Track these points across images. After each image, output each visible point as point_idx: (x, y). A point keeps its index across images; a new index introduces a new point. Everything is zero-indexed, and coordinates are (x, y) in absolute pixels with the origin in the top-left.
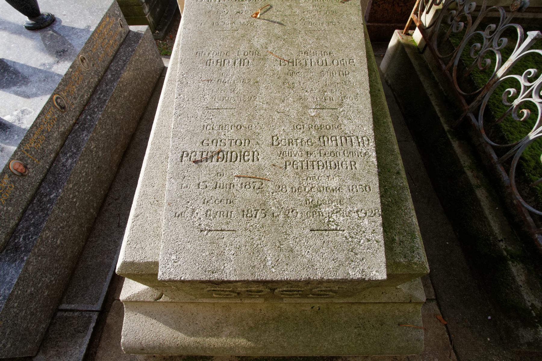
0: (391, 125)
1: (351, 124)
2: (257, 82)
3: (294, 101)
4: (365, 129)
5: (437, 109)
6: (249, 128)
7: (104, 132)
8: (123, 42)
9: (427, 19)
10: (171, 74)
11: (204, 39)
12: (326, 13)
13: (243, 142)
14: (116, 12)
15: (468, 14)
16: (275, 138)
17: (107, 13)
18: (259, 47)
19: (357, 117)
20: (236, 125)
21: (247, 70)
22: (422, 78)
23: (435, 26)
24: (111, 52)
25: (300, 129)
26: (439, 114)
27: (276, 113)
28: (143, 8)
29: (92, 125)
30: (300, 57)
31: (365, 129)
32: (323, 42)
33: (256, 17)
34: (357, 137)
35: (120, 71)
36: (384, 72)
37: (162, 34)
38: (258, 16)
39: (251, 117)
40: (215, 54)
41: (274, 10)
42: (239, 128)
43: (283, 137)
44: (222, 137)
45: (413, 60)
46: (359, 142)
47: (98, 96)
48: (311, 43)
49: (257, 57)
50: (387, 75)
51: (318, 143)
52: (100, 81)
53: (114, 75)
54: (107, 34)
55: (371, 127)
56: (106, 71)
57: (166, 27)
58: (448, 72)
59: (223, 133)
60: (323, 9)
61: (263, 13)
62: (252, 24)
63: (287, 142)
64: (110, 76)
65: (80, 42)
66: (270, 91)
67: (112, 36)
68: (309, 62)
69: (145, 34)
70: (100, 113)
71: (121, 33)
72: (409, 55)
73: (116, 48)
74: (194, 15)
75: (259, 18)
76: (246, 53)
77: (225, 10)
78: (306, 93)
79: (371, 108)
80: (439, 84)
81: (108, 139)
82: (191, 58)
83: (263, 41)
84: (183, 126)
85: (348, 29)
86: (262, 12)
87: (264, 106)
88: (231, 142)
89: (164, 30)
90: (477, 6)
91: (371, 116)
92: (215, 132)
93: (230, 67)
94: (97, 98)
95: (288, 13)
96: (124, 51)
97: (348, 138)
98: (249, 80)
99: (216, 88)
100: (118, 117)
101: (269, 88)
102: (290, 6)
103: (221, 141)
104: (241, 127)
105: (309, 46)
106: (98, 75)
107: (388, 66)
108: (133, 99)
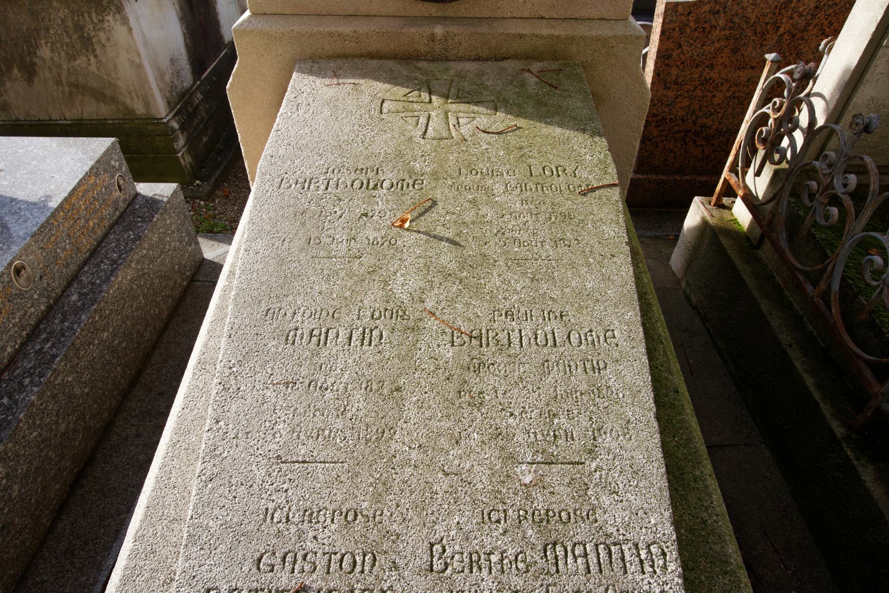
0: (713, 484)
1: (619, 505)
2: (398, 389)
3: (483, 442)
4: (653, 521)
5: (809, 381)
6: (373, 519)
7: (35, 434)
8: (117, 220)
9: (759, 184)
10: (206, 345)
11: (286, 276)
12: (550, 218)
13: (359, 559)
14: (113, 163)
15: (844, 194)
16: (437, 548)
17: (92, 168)
18: (405, 297)
19: (624, 326)
20: (344, 510)
21: (377, 357)
22: (765, 306)
23: (778, 203)
24: (87, 243)
25: (498, 521)
26: (817, 395)
27: (440, 475)
28: (175, 140)
29: (9, 422)
30: (495, 326)
31: (653, 521)
32: (545, 286)
33: (401, 227)
34: (636, 546)
35: (100, 285)
36: (679, 275)
37: (207, 187)
38: (407, 225)
39: (380, 487)
40: (308, 313)
41: (441, 211)
42: (350, 517)
43: (457, 548)
44: (310, 545)
45: (739, 263)
46: (641, 562)
47: (38, 347)
48: (519, 289)
49: (400, 324)
50: (688, 284)
51: (541, 563)
52: (50, 308)
53: (86, 294)
54: (86, 209)
55: (667, 514)
56: (69, 285)
57: (218, 173)
58: (819, 301)
59: (311, 534)
60: (543, 208)
61: (417, 218)
62: (393, 242)
63: (467, 560)
64: (74, 298)
65: (21, 233)
66: (428, 414)
67: (95, 211)
68: (515, 341)
69: (168, 202)
70: (35, 389)
71: (116, 201)
72: (729, 252)
73: (100, 233)
74: (270, 219)
75: (408, 230)
76: (377, 314)
77: (337, 209)
78: (511, 420)
79: (662, 461)
80: (805, 319)
81: (42, 450)
82: (253, 323)
83: (415, 283)
84: (216, 511)
85: (598, 258)
86: (415, 214)
87: (414, 455)
88: (330, 560)
89: (214, 178)
90: (859, 185)
91: (664, 483)
92: (293, 529)
93: (339, 348)
94: (36, 352)
95: (469, 217)
96: (118, 240)
97: (613, 548)
98: (381, 382)
99: (304, 404)
100: (77, 391)
101: (425, 405)
102: (474, 202)
103: (305, 557)
104: (356, 515)
105: (516, 297)
106: (49, 297)
107: (688, 266)
108: (120, 343)
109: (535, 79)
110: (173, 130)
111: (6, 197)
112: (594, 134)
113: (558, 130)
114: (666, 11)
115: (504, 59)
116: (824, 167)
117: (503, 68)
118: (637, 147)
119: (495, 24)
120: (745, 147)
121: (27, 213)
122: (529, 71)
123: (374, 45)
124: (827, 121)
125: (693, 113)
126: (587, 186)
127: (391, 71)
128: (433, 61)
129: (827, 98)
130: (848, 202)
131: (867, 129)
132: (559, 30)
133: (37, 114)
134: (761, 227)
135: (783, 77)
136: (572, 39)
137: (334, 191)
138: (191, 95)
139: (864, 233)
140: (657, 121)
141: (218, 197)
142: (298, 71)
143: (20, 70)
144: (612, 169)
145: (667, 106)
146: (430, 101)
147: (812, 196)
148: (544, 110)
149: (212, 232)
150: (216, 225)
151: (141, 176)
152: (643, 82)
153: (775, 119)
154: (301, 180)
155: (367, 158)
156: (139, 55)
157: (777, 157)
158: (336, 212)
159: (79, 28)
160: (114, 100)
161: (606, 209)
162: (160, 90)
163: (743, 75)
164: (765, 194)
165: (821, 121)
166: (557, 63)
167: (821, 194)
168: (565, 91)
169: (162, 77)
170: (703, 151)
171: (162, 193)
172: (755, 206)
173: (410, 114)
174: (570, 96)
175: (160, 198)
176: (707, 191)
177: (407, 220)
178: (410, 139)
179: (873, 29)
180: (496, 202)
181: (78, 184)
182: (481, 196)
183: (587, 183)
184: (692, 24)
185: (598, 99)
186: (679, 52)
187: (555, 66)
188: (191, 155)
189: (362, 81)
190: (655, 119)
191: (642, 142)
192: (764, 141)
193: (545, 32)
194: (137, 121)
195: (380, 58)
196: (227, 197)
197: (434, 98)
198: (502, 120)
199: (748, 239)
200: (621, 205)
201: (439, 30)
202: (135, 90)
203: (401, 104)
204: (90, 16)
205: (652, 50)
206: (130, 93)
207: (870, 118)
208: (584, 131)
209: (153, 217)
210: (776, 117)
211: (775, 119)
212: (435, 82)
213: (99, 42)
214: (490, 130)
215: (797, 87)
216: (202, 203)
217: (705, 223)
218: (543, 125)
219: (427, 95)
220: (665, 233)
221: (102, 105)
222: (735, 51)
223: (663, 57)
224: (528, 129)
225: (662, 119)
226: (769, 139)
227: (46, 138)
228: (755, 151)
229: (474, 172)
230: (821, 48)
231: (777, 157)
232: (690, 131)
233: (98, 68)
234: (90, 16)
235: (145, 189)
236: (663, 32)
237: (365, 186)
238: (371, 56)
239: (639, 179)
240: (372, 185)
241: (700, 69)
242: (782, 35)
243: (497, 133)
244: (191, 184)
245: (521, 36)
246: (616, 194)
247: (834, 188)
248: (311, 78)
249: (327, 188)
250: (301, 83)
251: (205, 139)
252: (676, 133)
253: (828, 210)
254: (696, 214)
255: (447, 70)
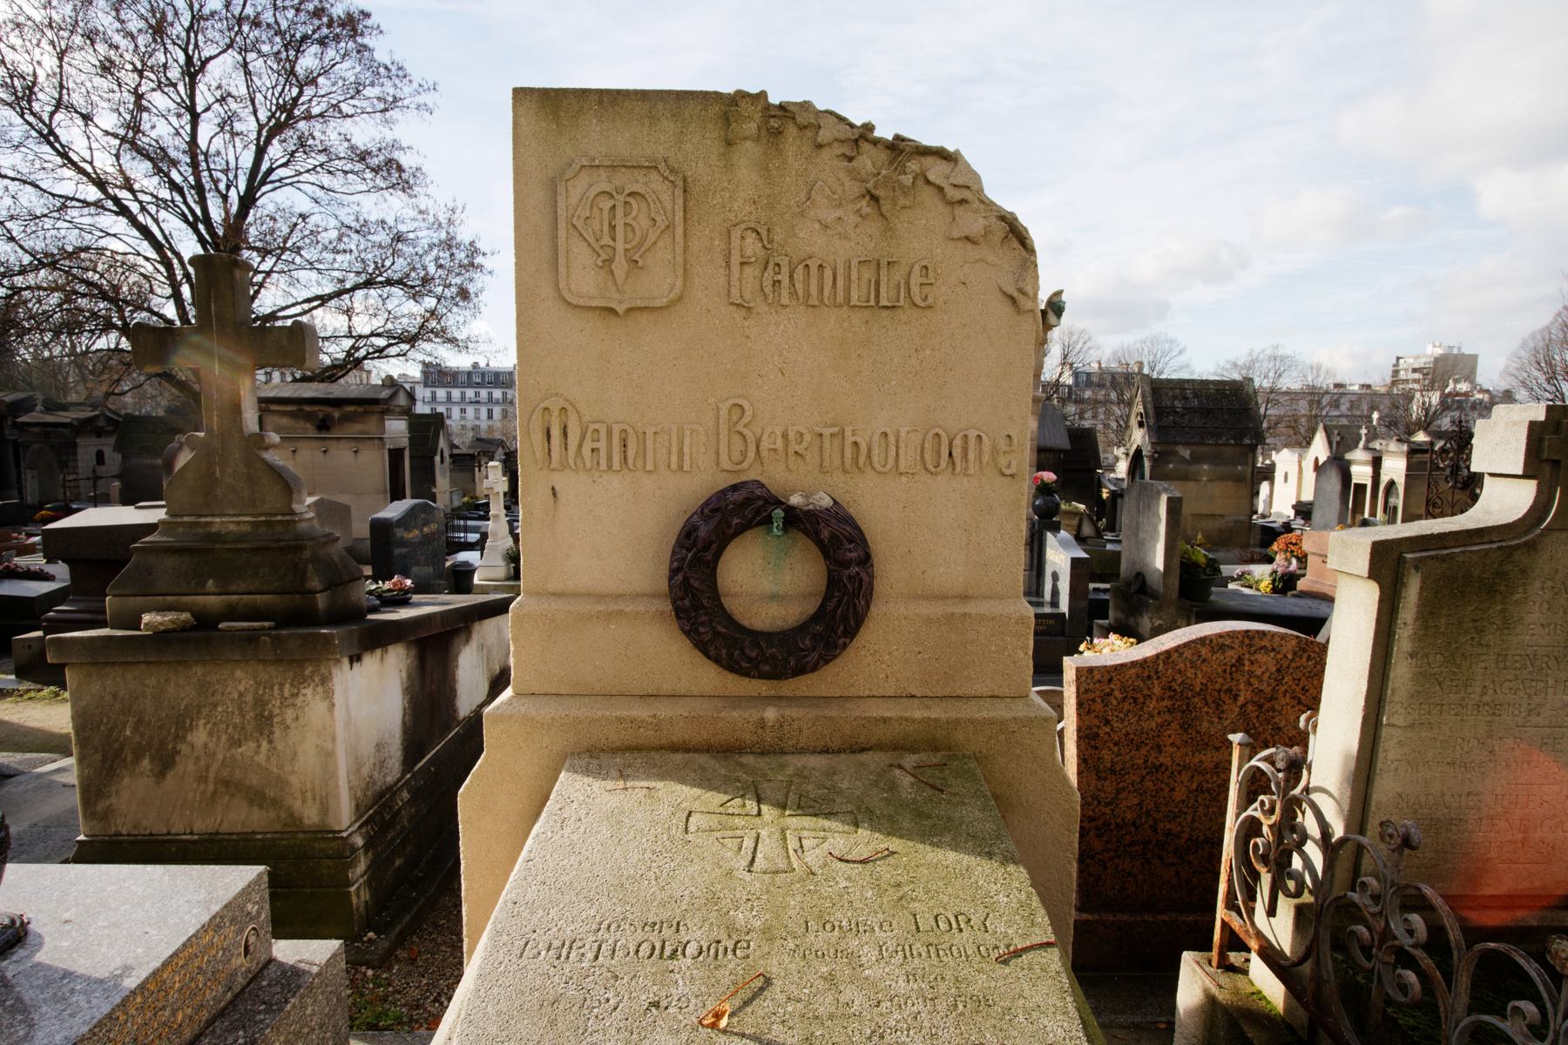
9: (1281, 929)
15: (1415, 946)
28: (352, 864)
33: (713, 1026)
38: (723, 1023)
60: (943, 988)
61: (740, 1009)
69: (319, 974)
74: (499, 1013)
75: (725, 1032)
77: (610, 995)
86: (737, 1002)
102: (830, 978)
109: (908, 779)
110: (354, 849)
111: (56, 970)
112: (1007, 859)
113: (952, 856)
114: (1078, 679)
115: (863, 750)
116: (1368, 902)
117: (862, 764)
118: (1075, 875)
119: (848, 705)
120: (1239, 869)
121: (82, 997)
122: (900, 767)
123: (678, 734)
124: (1347, 828)
125: (1148, 814)
126: (1008, 946)
127: (703, 769)
128: (762, 754)
129: (1336, 794)
130: (1426, 962)
131: (1407, 842)
132: (936, 712)
133: (153, 825)
134: (1305, 1006)
135: (1263, 766)
136: (957, 722)
137: (608, 962)
138: (394, 794)
139: (1473, 1018)
140: (1097, 828)
141: (398, 961)
142: (568, 770)
143: (153, 760)
144: (1042, 917)
145: (1110, 804)
146: (759, 814)
147: (1366, 950)
148: (924, 820)
149: (373, 1027)
150: (385, 1014)
151: (285, 926)
152: (1065, 779)
153: (1271, 827)
154: (557, 943)
155: (663, 904)
156: (334, 740)
157: (1291, 885)
158: (608, 1000)
159: (260, 703)
160: (276, 803)
161: (1042, 988)
162: (351, 788)
163: (1208, 758)
164: (1293, 947)
165: (1338, 831)
166: (939, 755)
167: (1380, 948)
168: (955, 795)
169: (358, 770)
170: (1177, 873)
171: (311, 959)
172: (1280, 967)
173: (730, 833)
174: (964, 803)
175: (307, 967)
176: (1203, 944)
177: (723, 1013)
178: (730, 873)
179: (1362, 703)
180: (866, 978)
181: (184, 945)
182: (842, 969)
183: (1006, 941)
184: (1117, 693)
185: (1003, 802)
186: (1107, 729)
187: (936, 758)
188: (370, 887)
189: (659, 785)
190: (1093, 824)
191: (1081, 861)
192: (1264, 859)
193: (918, 714)
194: (301, 836)
195: (687, 750)
196: (413, 961)
197: (764, 808)
198: (865, 841)
199: (1289, 1027)
200: (1065, 980)
201: (771, 714)
202: (313, 789)
203: (716, 818)
204: (281, 689)
205: (1070, 724)
206: (303, 793)
207: (1404, 826)
208: (990, 855)
209: (287, 1002)
210: (1271, 822)
211: (1271, 827)
212: (765, 785)
213: (283, 722)
214: (849, 857)
215: (1287, 780)
216: (370, 972)
217: (1211, 1000)
218: (928, 848)
219: (755, 804)
220: (1149, 1018)
221: (256, 809)
222: (1185, 727)
223: (1087, 736)
224: (907, 854)
225: (1104, 824)
226: (1272, 856)
227: (158, 867)
228: (1256, 876)
229: (828, 927)
230: (1302, 724)
231: (1291, 885)
232: (1149, 842)
233: (268, 758)
234: (281, 689)
235: (287, 951)
236: (1080, 705)
237: (657, 952)
238: (675, 748)
239: (1087, 921)
240: (667, 953)
241: (1143, 751)
242: (1244, 705)
243: (861, 862)
244: (359, 938)
245: (885, 720)
246: (1054, 960)
247: (1395, 938)
248: (586, 780)
249: (596, 957)
250: (569, 785)
251: (398, 862)
252: (1131, 844)
253: (1400, 976)
254: (1193, 983)
255: (782, 766)
